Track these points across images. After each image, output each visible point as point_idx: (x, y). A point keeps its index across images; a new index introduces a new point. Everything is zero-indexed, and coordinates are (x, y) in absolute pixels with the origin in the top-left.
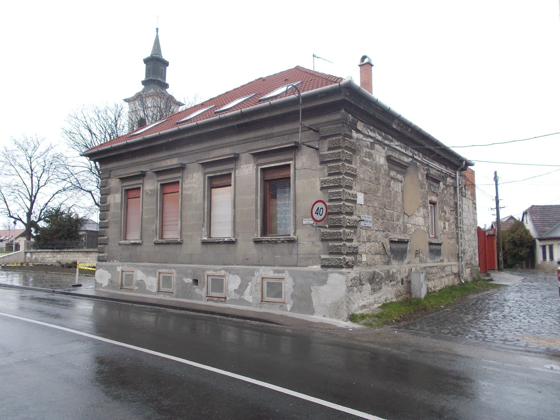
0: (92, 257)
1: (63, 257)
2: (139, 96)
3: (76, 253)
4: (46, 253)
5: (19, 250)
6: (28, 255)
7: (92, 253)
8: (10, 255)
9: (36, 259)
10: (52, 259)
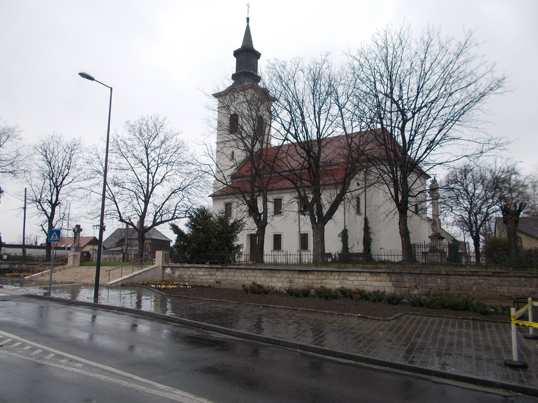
0: (281, 277)
1: (227, 276)
2: (230, 91)
3: (250, 271)
4: (197, 270)
5: (153, 264)
6: (168, 271)
7: (281, 272)
8: (147, 270)
9: (180, 276)
10: (209, 277)
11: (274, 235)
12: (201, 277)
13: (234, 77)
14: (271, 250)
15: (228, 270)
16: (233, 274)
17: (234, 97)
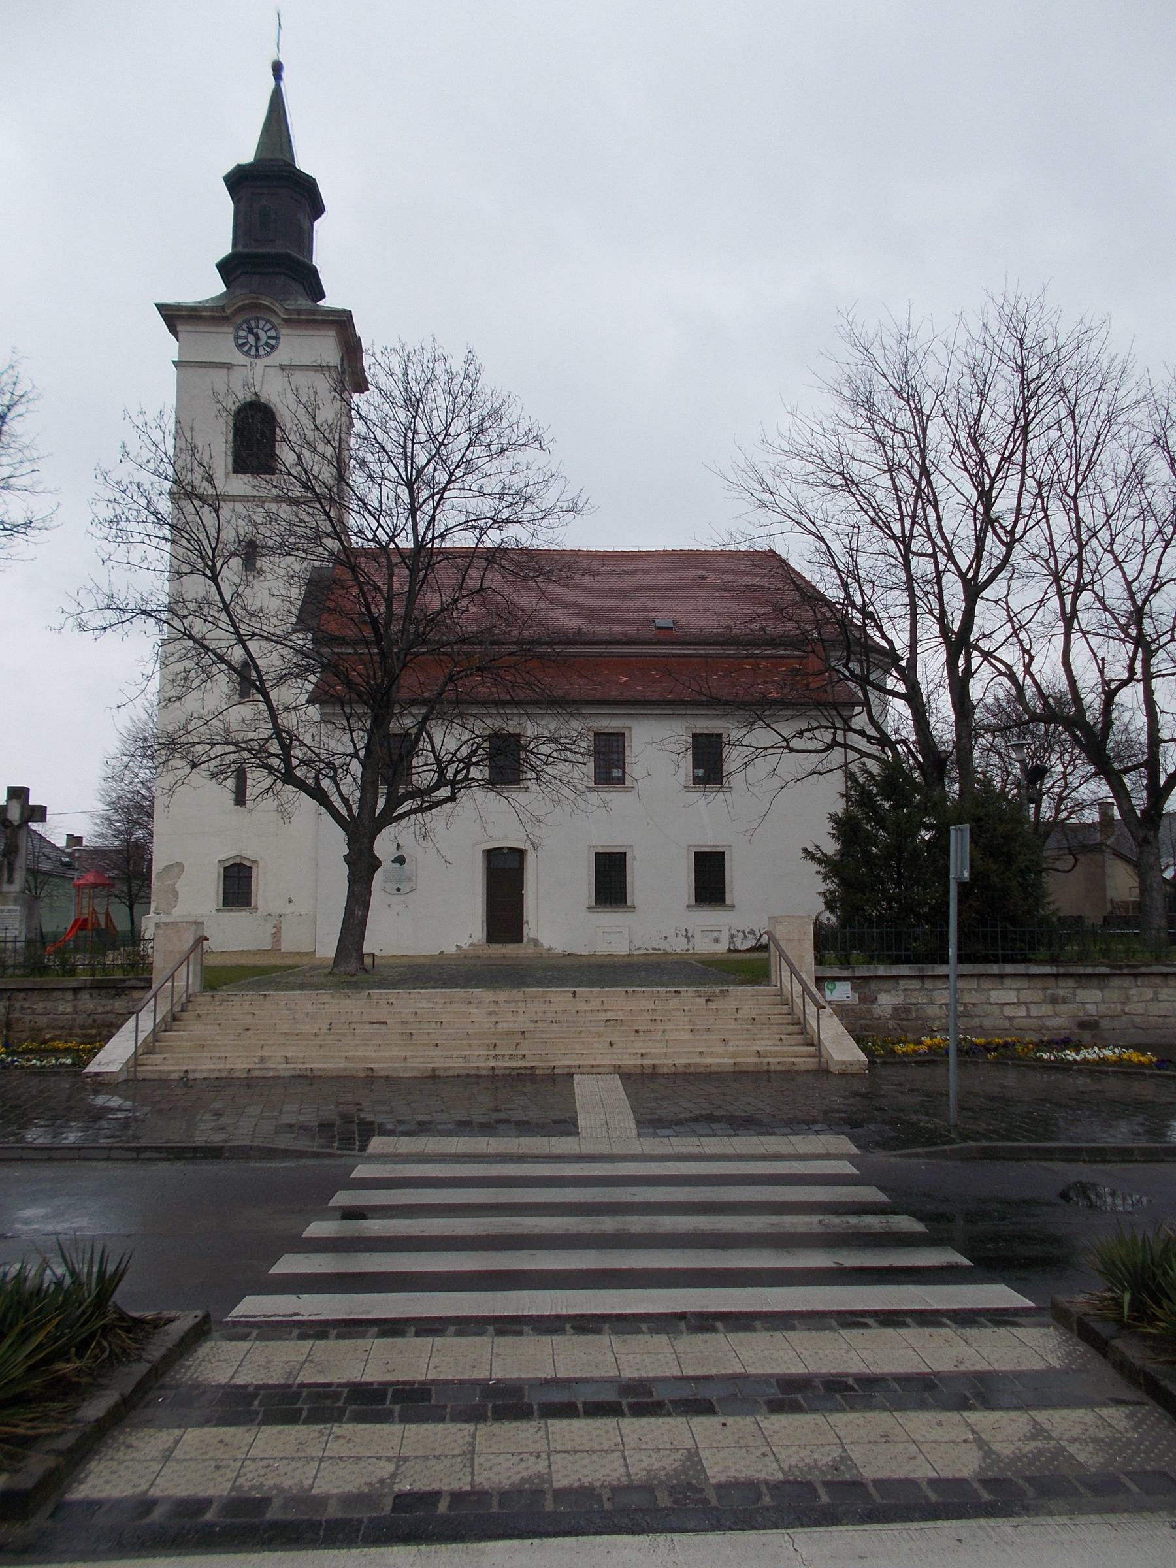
9: (901, 1012)
10: (1046, 1009)
11: (696, 854)
12: (1008, 1011)
13: (225, 268)
14: (587, 904)
15: (1127, 982)
16: (1149, 994)
17: (258, 338)
